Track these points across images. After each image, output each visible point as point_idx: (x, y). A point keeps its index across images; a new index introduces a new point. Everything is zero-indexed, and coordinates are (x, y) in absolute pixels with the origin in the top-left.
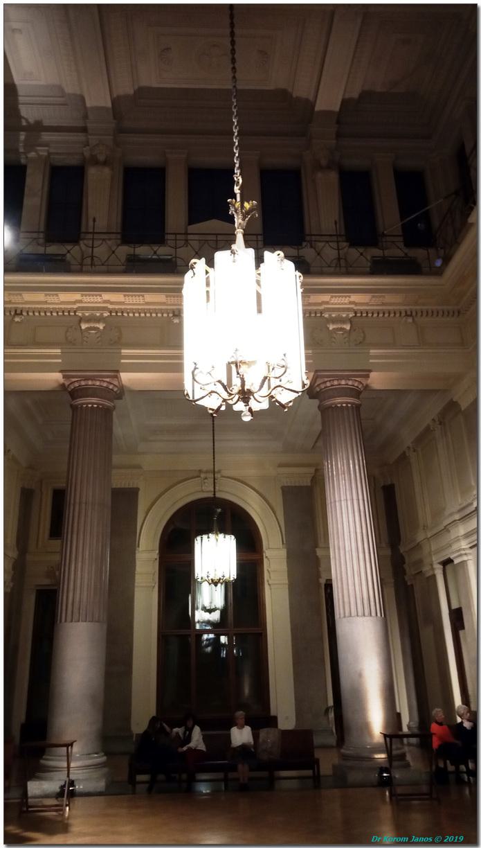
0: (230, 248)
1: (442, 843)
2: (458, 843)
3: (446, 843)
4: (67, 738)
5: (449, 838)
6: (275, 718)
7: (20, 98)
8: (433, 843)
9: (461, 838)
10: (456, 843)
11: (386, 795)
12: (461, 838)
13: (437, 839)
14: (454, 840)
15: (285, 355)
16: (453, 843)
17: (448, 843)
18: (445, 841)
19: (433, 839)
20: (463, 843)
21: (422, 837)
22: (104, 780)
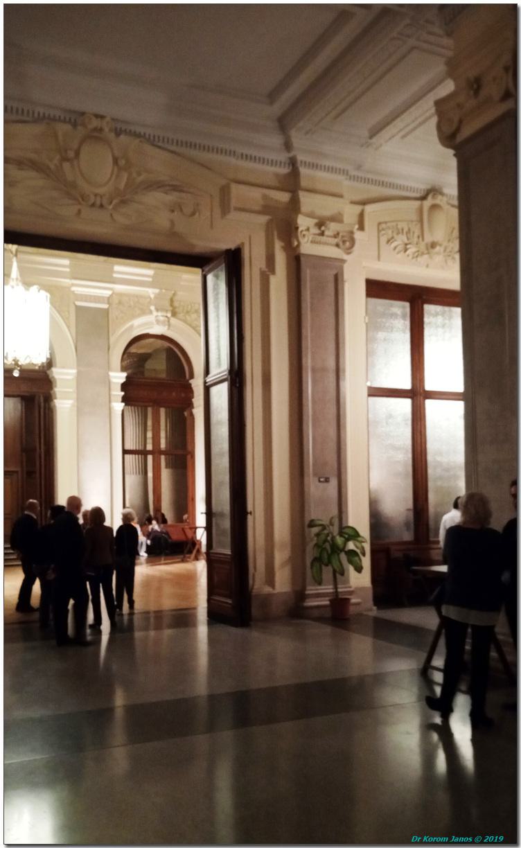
0: (41, 289)
1: (482, 843)
2: (498, 843)
3: (485, 843)
4: (18, 256)
5: (488, 838)
6: (131, 392)
7: (137, 449)
8: (473, 843)
9: (502, 838)
10: (496, 843)
11: (473, 645)
12: (502, 838)
13: (477, 840)
14: (494, 839)
15: (15, 351)
16: (493, 843)
17: (488, 843)
18: (485, 841)
19: (473, 839)
20: (504, 842)
21: (444, 837)
22: (125, 374)
